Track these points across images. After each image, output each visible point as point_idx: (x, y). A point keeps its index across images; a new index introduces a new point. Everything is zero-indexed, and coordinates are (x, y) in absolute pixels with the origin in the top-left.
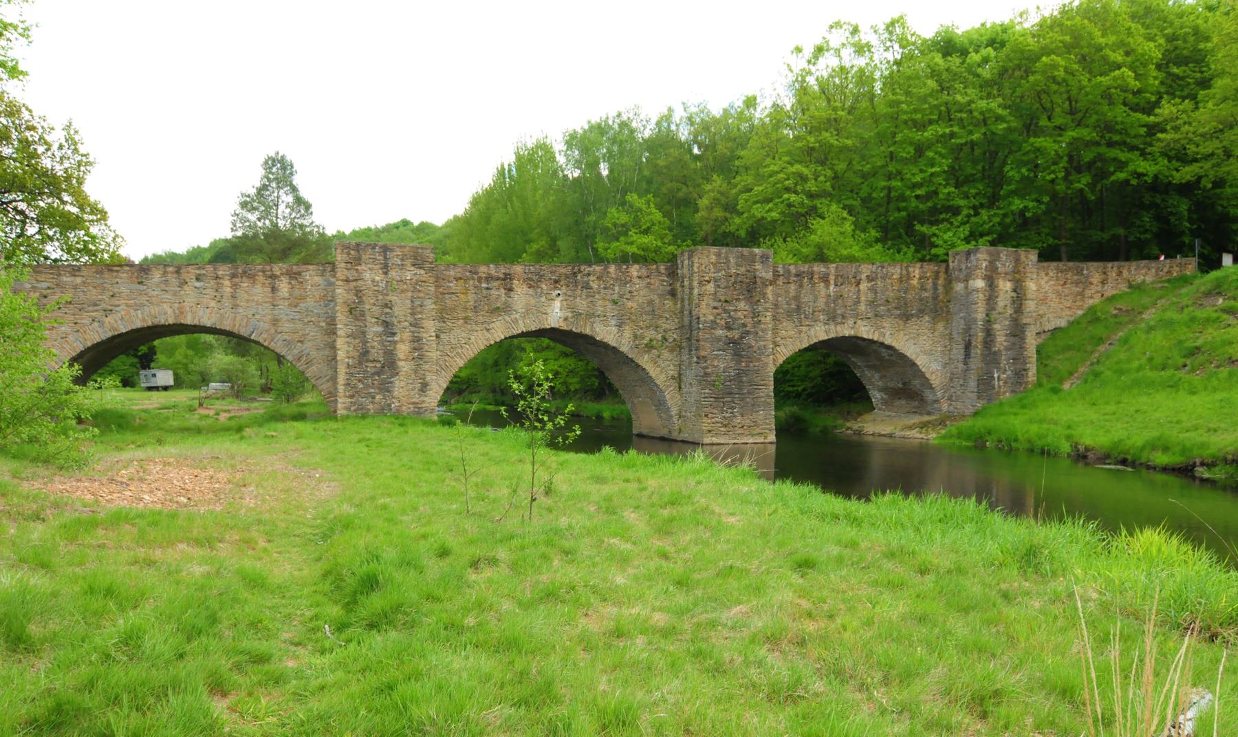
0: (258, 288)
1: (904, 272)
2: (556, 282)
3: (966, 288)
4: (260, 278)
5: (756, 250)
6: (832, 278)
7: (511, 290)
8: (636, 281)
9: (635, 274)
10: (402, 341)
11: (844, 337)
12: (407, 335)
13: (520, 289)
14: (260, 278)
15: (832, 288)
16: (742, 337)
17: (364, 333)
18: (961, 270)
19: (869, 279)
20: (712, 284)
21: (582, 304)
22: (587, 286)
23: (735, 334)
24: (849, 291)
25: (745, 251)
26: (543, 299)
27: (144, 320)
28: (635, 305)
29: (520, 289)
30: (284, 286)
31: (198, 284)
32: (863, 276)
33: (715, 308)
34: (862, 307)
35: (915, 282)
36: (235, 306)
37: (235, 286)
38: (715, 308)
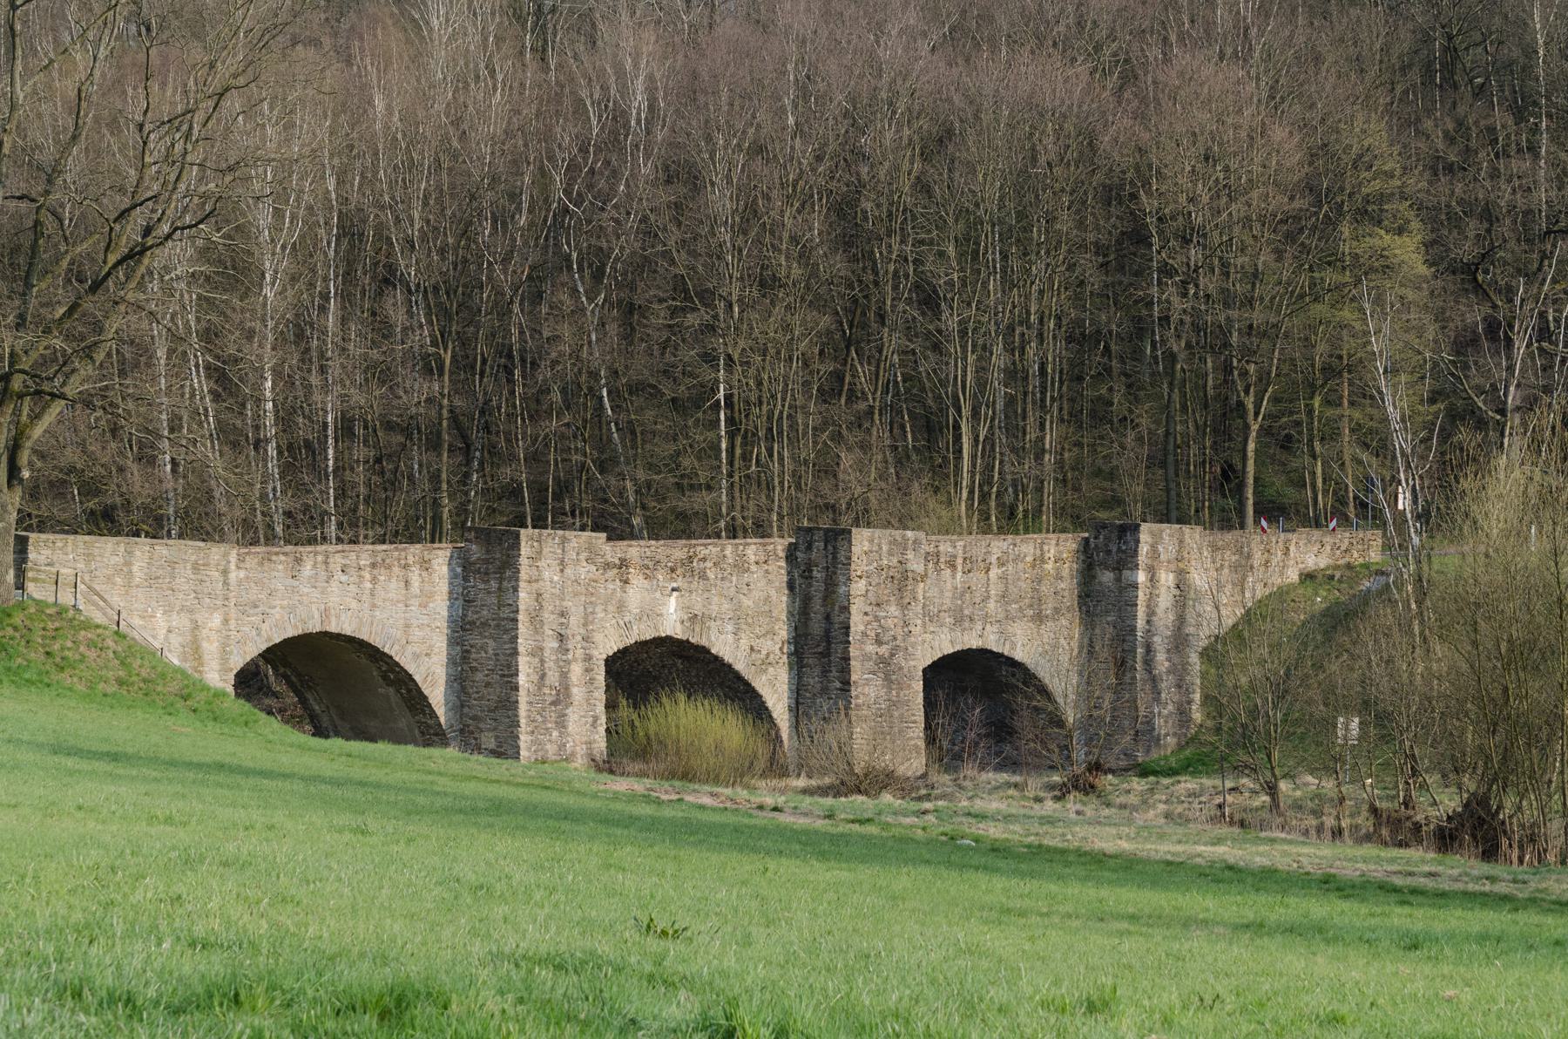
0: (394, 584)
1: (1038, 552)
2: (673, 570)
3: (1118, 580)
4: (396, 569)
5: (909, 534)
6: (959, 561)
7: (626, 582)
8: (753, 568)
9: (753, 558)
10: (575, 660)
11: (970, 650)
12: (580, 652)
13: (637, 580)
14: (396, 569)
15: (959, 574)
16: (892, 655)
17: (542, 649)
18: (1109, 552)
19: (1001, 563)
20: (863, 582)
21: (697, 603)
22: (703, 576)
23: (884, 650)
24: (977, 578)
25: (898, 534)
26: (658, 595)
27: (296, 627)
28: (750, 603)
29: (637, 580)
30: (415, 577)
31: (344, 578)
32: (993, 559)
33: (866, 614)
34: (992, 605)
35: (1049, 566)
36: (374, 606)
37: (374, 580)
38: (866, 614)
